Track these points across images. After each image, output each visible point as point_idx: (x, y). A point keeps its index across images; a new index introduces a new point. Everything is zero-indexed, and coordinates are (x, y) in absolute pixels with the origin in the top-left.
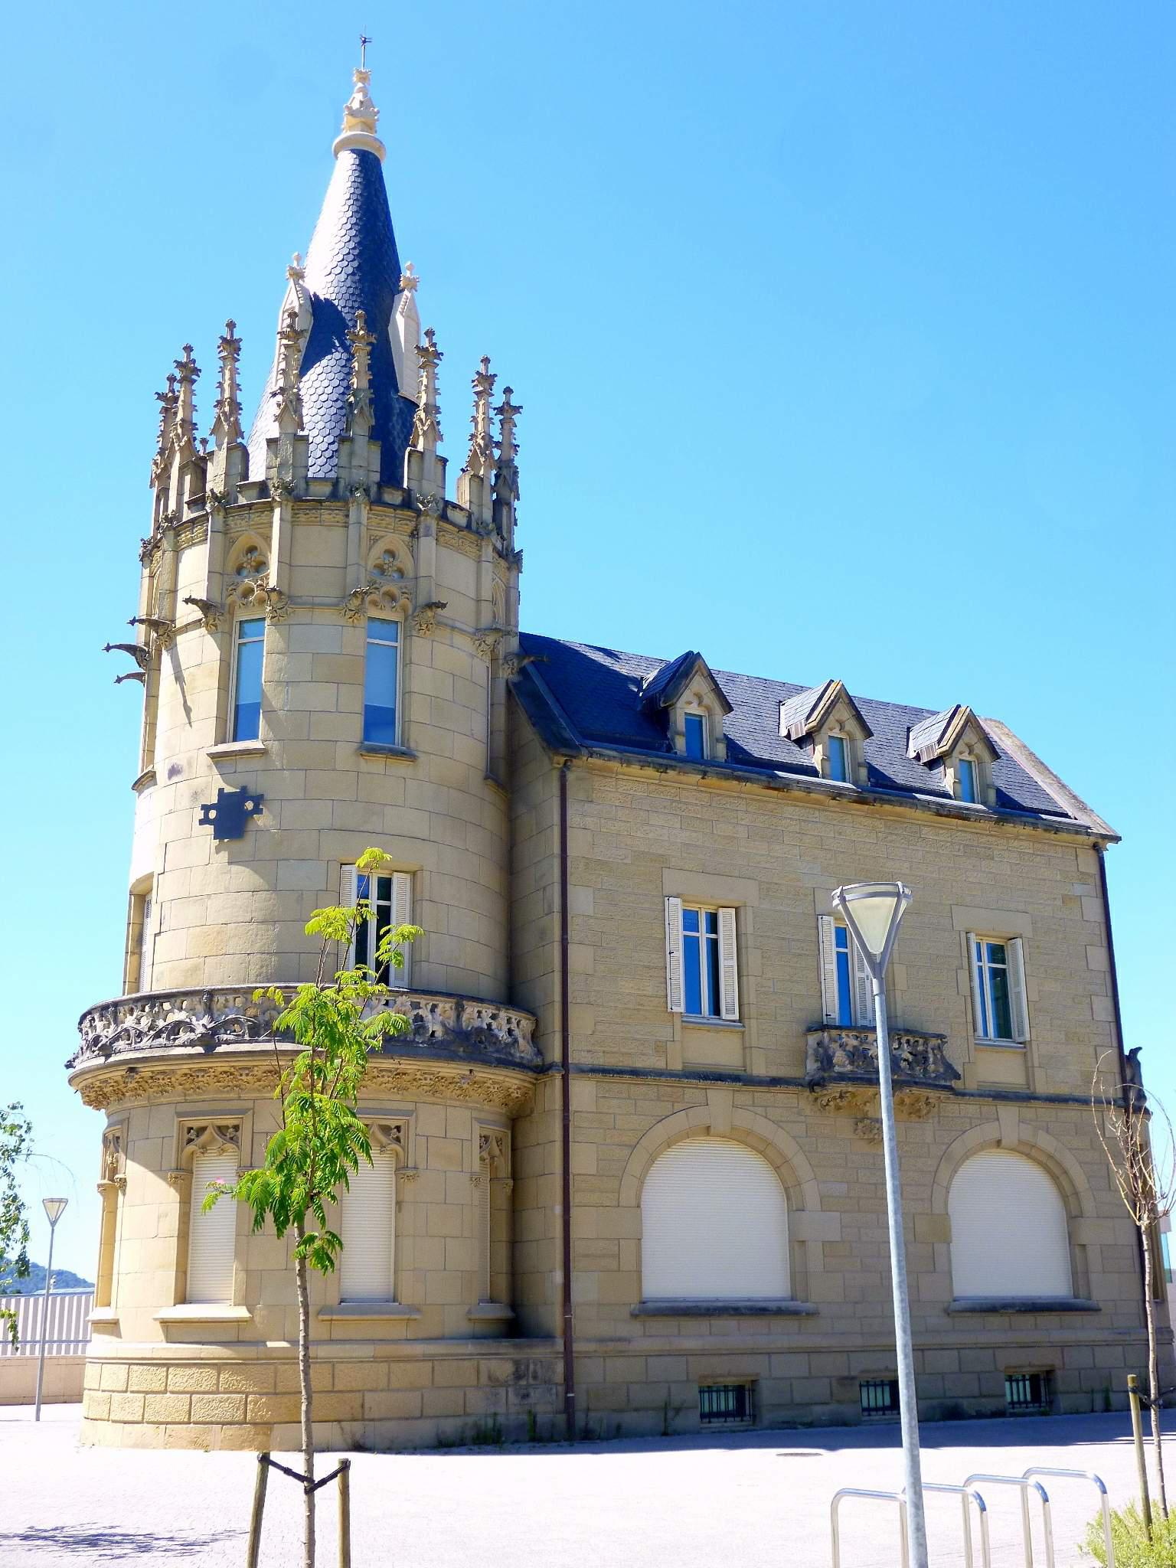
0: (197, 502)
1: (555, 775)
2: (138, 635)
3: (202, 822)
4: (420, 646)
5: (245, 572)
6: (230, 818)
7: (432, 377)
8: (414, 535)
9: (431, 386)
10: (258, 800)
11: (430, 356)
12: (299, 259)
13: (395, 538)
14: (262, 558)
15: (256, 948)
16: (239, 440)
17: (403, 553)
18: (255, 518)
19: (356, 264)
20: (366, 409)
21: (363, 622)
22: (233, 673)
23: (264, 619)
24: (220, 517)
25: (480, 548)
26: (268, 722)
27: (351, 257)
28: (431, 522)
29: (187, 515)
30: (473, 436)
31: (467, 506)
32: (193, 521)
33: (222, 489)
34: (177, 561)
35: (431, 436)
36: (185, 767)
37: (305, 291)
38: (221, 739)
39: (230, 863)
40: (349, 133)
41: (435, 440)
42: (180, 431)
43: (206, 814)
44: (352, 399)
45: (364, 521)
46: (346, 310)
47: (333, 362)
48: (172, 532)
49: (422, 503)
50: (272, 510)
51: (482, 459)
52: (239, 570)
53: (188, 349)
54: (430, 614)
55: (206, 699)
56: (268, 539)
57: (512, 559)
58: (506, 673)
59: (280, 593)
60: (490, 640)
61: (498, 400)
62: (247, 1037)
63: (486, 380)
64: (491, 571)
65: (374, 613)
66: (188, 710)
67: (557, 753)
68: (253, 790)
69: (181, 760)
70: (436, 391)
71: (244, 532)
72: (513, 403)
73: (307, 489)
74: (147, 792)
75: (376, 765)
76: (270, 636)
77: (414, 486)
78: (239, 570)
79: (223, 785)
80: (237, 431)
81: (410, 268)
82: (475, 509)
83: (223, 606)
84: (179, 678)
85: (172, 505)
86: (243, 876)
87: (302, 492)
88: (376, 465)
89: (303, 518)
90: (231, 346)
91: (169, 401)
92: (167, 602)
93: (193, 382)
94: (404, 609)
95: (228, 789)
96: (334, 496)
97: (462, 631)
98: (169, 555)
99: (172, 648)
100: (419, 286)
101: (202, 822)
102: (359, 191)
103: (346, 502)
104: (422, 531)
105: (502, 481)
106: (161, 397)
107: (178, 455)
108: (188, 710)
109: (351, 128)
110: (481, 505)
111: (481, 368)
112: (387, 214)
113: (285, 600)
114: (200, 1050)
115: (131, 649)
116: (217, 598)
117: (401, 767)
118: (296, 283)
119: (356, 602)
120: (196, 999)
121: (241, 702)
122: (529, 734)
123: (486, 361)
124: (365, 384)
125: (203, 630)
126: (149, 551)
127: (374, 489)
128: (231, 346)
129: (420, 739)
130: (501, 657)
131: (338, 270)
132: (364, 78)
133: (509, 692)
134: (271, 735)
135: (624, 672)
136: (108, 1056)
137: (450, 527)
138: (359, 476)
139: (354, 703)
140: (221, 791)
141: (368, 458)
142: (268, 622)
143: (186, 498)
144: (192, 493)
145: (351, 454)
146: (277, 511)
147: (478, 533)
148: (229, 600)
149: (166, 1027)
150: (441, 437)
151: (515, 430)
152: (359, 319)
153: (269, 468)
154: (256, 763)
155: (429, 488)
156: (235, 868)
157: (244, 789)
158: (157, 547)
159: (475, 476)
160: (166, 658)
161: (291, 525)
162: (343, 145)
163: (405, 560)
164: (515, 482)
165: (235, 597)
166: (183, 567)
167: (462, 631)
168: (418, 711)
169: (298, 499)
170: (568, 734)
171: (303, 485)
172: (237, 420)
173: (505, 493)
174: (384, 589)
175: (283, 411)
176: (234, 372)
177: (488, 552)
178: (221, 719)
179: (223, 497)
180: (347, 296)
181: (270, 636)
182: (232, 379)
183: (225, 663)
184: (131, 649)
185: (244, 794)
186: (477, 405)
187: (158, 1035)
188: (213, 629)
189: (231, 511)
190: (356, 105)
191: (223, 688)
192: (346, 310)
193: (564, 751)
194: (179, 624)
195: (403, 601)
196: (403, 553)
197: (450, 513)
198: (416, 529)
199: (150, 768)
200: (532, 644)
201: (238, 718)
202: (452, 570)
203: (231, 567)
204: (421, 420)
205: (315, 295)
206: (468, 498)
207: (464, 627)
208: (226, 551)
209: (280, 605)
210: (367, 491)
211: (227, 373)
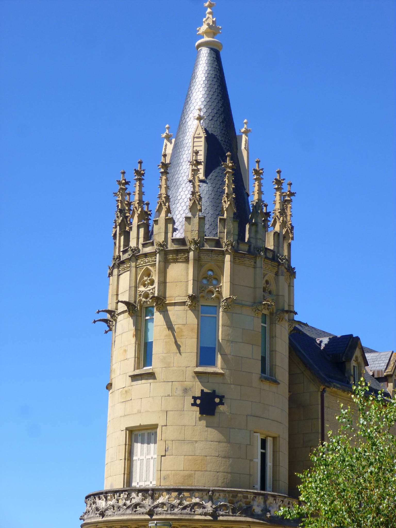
3: (193, 405)
6: (207, 404)
8: (277, 274)
10: (222, 398)
15: (221, 469)
17: (272, 282)
27: (220, 112)
39: (207, 426)
43: (195, 401)
49: (280, 259)
55: (190, 344)
62: (231, 514)
68: (218, 392)
75: (266, 386)
79: (203, 388)
86: (213, 434)
89: (238, 261)
95: (206, 390)
101: (193, 405)
104: (280, 272)
108: (178, 347)
114: (209, 518)
120: (205, 493)
134: (225, 367)
136: (103, 517)
140: (202, 391)
149: (131, 505)
155: (259, 243)
156: (210, 429)
157: (214, 391)
161: (233, 262)
163: (273, 287)
179: (198, 243)
185: (213, 394)
187: (185, 508)
188: (193, 308)
196: (272, 282)
207: (247, 303)
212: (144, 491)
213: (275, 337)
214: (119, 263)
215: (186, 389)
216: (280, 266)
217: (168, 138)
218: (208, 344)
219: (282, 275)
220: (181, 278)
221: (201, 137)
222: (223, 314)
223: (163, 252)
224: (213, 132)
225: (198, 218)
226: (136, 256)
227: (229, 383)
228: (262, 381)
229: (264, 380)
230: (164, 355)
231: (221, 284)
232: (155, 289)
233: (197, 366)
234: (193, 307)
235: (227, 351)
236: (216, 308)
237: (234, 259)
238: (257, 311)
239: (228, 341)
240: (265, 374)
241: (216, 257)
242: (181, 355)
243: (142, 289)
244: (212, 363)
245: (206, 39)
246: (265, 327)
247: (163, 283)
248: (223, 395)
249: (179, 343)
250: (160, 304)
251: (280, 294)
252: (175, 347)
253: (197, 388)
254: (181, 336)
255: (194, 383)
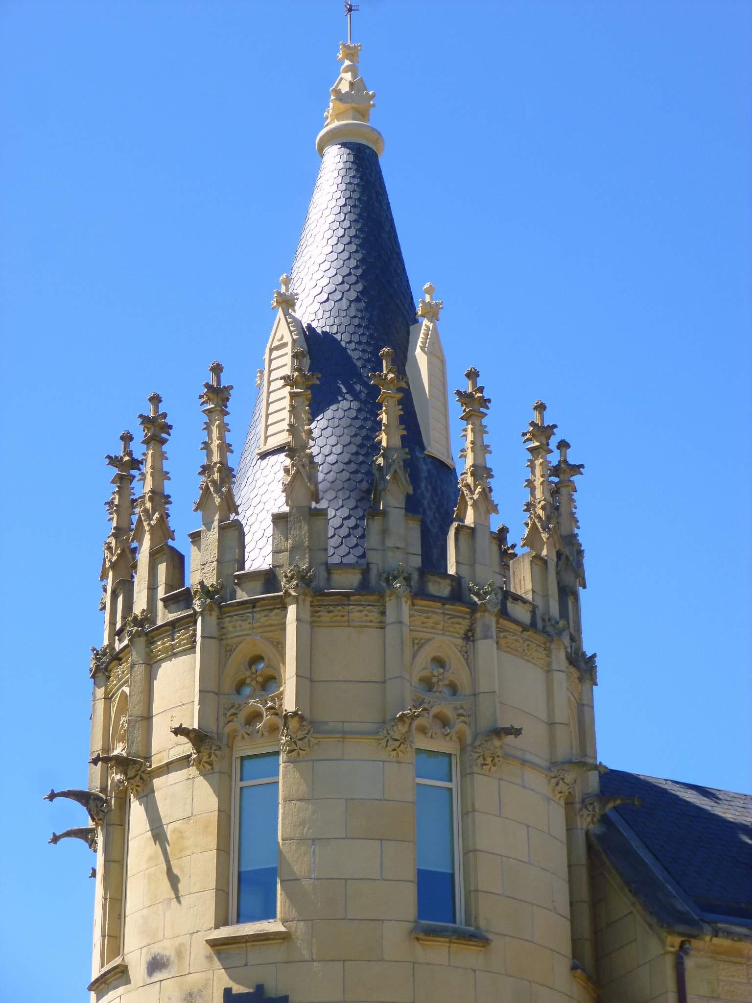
0: (180, 598)
1: (669, 963)
2: (91, 779)
4: (484, 787)
5: (247, 691)
7: (480, 431)
8: (469, 637)
9: (479, 443)
11: (475, 405)
12: (287, 281)
13: (445, 642)
14: (271, 672)
16: (233, 517)
17: (455, 659)
18: (261, 618)
19: (359, 287)
20: (401, 473)
21: (410, 756)
22: (234, 829)
23: (277, 753)
24: (213, 619)
25: (549, 651)
26: (290, 895)
27: (353, 279)
28: (489, 619)
29: (163, 616)
30: (529, 506)
31: (529, 597)
32: (173, 625)
33: (213, 580)
34: (150, 677)
35: (482, 506)
36: (173, 958)
37: (297, 322)
38: (222, 921)
40: (336, 123)
41: (488, 512)
42: (148, 505)
44: (381, 461)
45: (406, 619)
46: (353, 346)
47: (340, 413)
48: (143, 639)
49: (477, 594)
50: (285, 608)
51: (544, 536)
52: (239, 687)
53: (156, 400)
54: (497, 743)
55: (200, 865)
56: (280, 646)
57: (584, 667)
58: (585, 822)
59: (302, 718)
60: (569, 777)
61: (554, 458)
63: (543, 431)
64: (563, 679)
65: (422, 743)
66: (174, 880)
67: (671, 932)
69: (165, 948)
70: (486, 449)
71: (247, 636)
72: (571, 461)
73: (328, 580)
74: (111, 995)
75: (438, 952)
76: (285, 776)
77: (465, 573)
78: (239, 687)
79: (230, 984)
80: (230, 505)
81: (429, 291)
82: (539, 602)
83: (220, 736)
84: (158, 834)
85: (140, 604)
87: (322, 584)
88: (417, 548)
89: (325, 617)
90: (218, 395)
91: (126, 468)
92: (138, 735)
93: (164, 441)
94: (461, 739)
95: (237, 989)
96: (364, 587)
97: (534, 766)
98: (140, 670)
99: (148, 797)
100: (442, 314)
102: (356, 195)
103: (382, 595)
105: (566, 566)
106: (114, 461)
107: (147, 539)
108: (174, 880)
109: (338, 116)
110: (546, 596)
111: (536, 417)
112: (392, 220)
113: (307, 727)
115: (82, 797)
116: (212, 727)
117: (469, 955)
118: (286, 314)
119: (403, 729)
121: (243, 869)
122: (624, 905)
123: (541, 408)
124: (397, 442)
125: (193, 771)
126: (105, 664)
127: (415, 576)
128: (218, 395)
129: (490, 916)
130: (578, 799)
131: (338, 295)
132: (351, 54)
133: (589, 847)
134: (294, 913)
135: (729, 816)
137: (513, 626)
138: (395, 560)
139: (403, 865)
140: (227, 992)
141: (401, 539)
142: (282, 758)
143: (161, 593)
144: (169, 587)
145: (385, 532)
146: (292, 610)
147: (544, 631)
148: (228, 729)
150: (495, 509)
151: (576, 496)
152: (358, 358)
153: (276, 552)
154: (276, 952)
157: (260, 988)
158: (117, 658)
159: (537, 557)
160: (137, 811)
161: (309, 627)
162: (331, 138)
163: (458, 671)
164: (580, 565)
165: (237, 724)
166: (159, 685)
167: (534, 766)
168: (487, 878)
169: (319, 593)
170: (681, 905)
171: (323, 574)
172: (230, 491)
173: (569, 578)
174: (435, 710)
175: (294, 478)
176: (224, 428)
177: (560, 658)
178: (221, 892)
179: (216, 592)
180: (351, 329)
181: (285, 776)
182: (221, 437)
183: (224, 814)
184: (82, 797)
186: (532, 466)
188: (206, 768)
189: (233, 607)
190: (344, 88)
191: (223, 849)
192: (353, 346)
193: (681, 928)
194: (156, 762)
195: (459, 726)
196: (455, 659)
197: (510, 606)
198: (471, 629)
199: (117, 961)
200: (617, 783)
201: (246, 887)
202: (514, 681)
203: (228, 685)
204: (467, 486)
205: (309, 326)
206: (529, 586)
207: (538, 761)
208: (222, 665)
209: (301, 735)
210: (408, 579)
211: (215, 430)
213: (474, 811)
215: (191, 995)
216: (478, 615)
218: (254, 862)
219: (486, 637)
221: (285, 345)
222: (286, 767)
223: (143, 639)
224: (327, 329)
225: (216, 530)
227: (307, 957)
228: (418, 939)
229: (421, 936)
230: (145, 912)
231: (282, 689)
233: (217, 927)
234: (208, 767)
237: (314, 613)
238: (391, 742)
239: (302, 840)
240: (454, 922)
241: (263, 620)
242: (179, 902)
246: (451, 790)
248: (284, 994)
249: (176, 871)
250: (132, 778)
252: (166, 883)
254: (181, 851)
255: (210, 974)
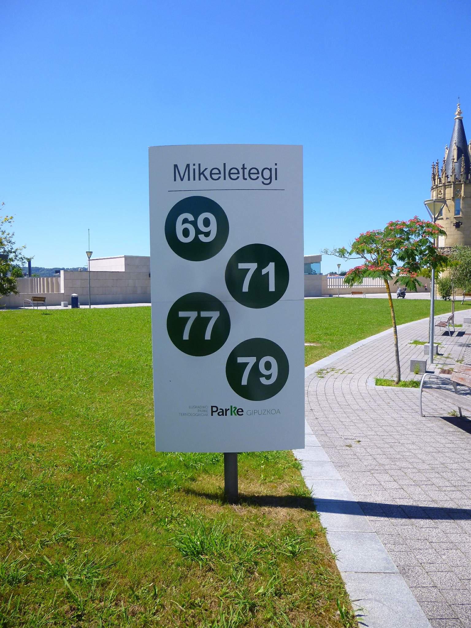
6: (457, 225)
55: (453, 209)
185: (459, 222)
212: (441, 248)
214: (433, 189)
217: (447, 148)
220: (449, 192)
226: (437, 187)
232: (442, 196)
235: (463, 210)
236: (460, 199)
243: (439, 196)
244: (459, 214)
245: (458, 117)
247: (445, 194)
251: (322, 484)
253: (455, 221)
